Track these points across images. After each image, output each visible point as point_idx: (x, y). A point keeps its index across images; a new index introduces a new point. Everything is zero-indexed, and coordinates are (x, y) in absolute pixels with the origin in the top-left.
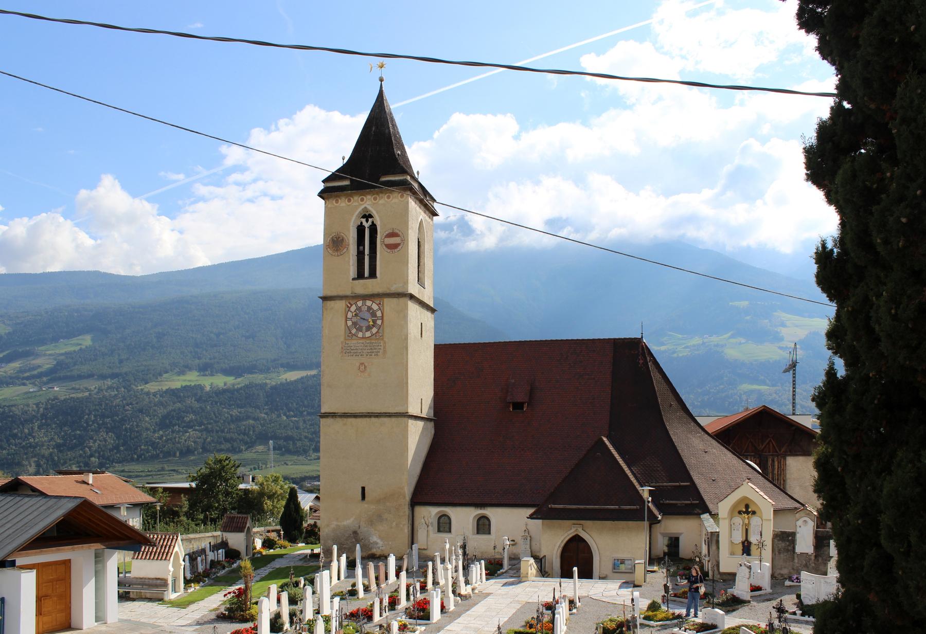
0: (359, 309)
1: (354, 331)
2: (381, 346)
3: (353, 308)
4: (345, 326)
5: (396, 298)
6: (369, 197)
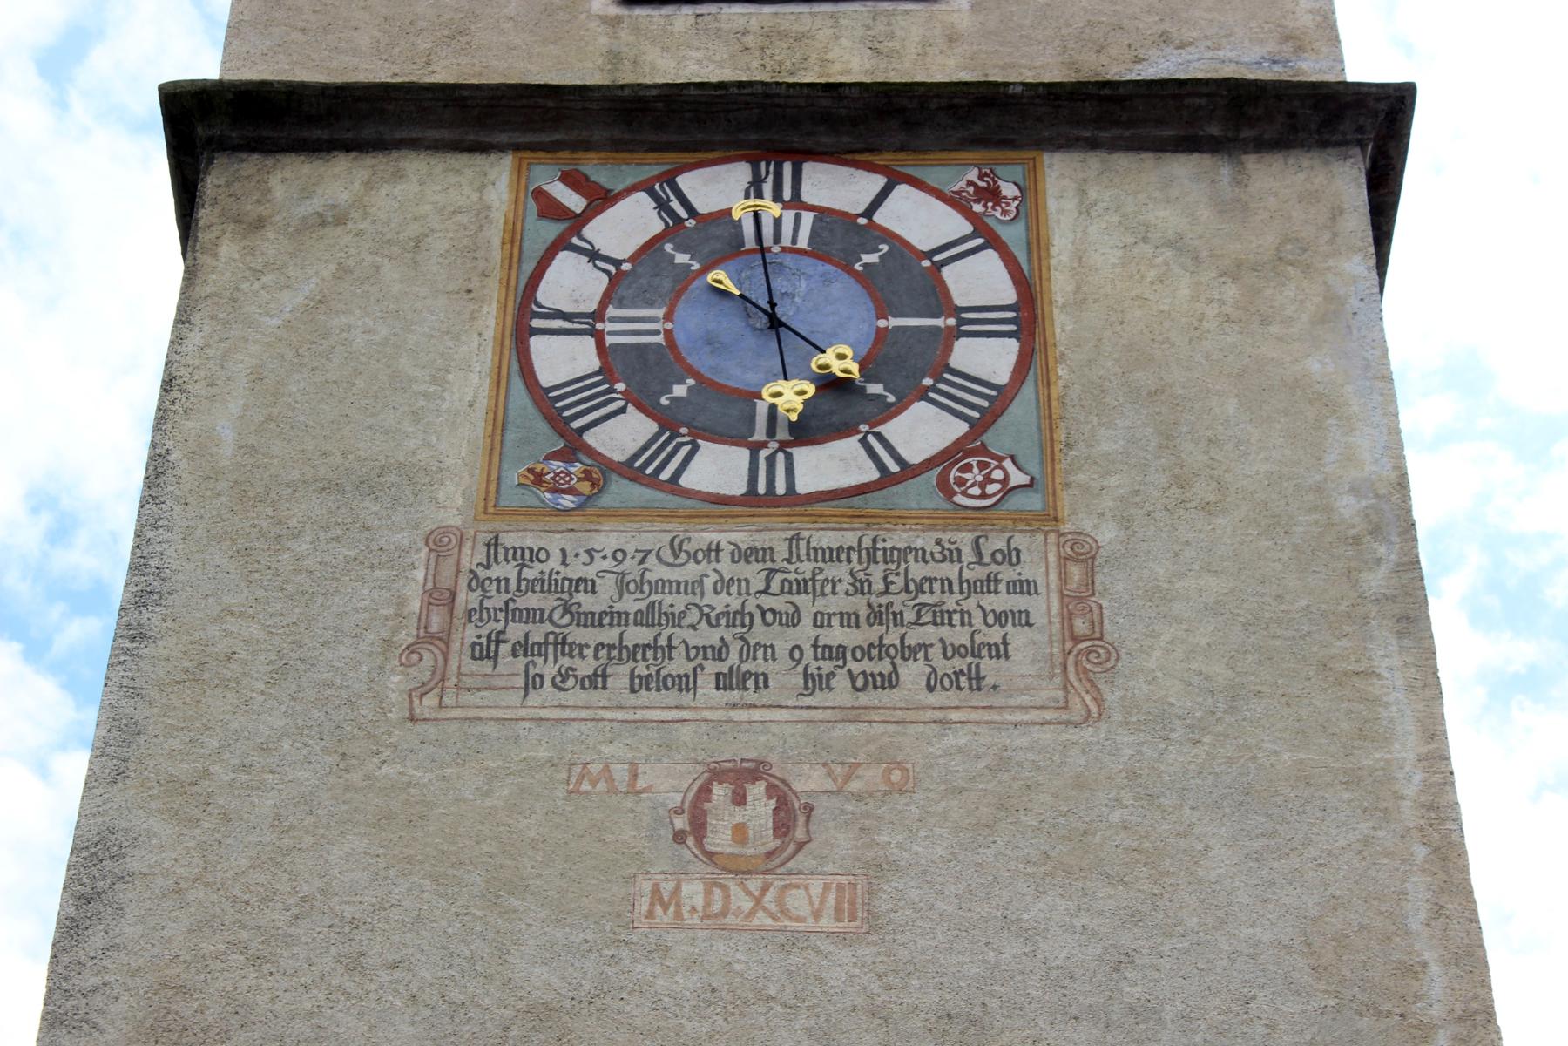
2: (1024, 587)
4: (499, 380)
5: (1212, 146)
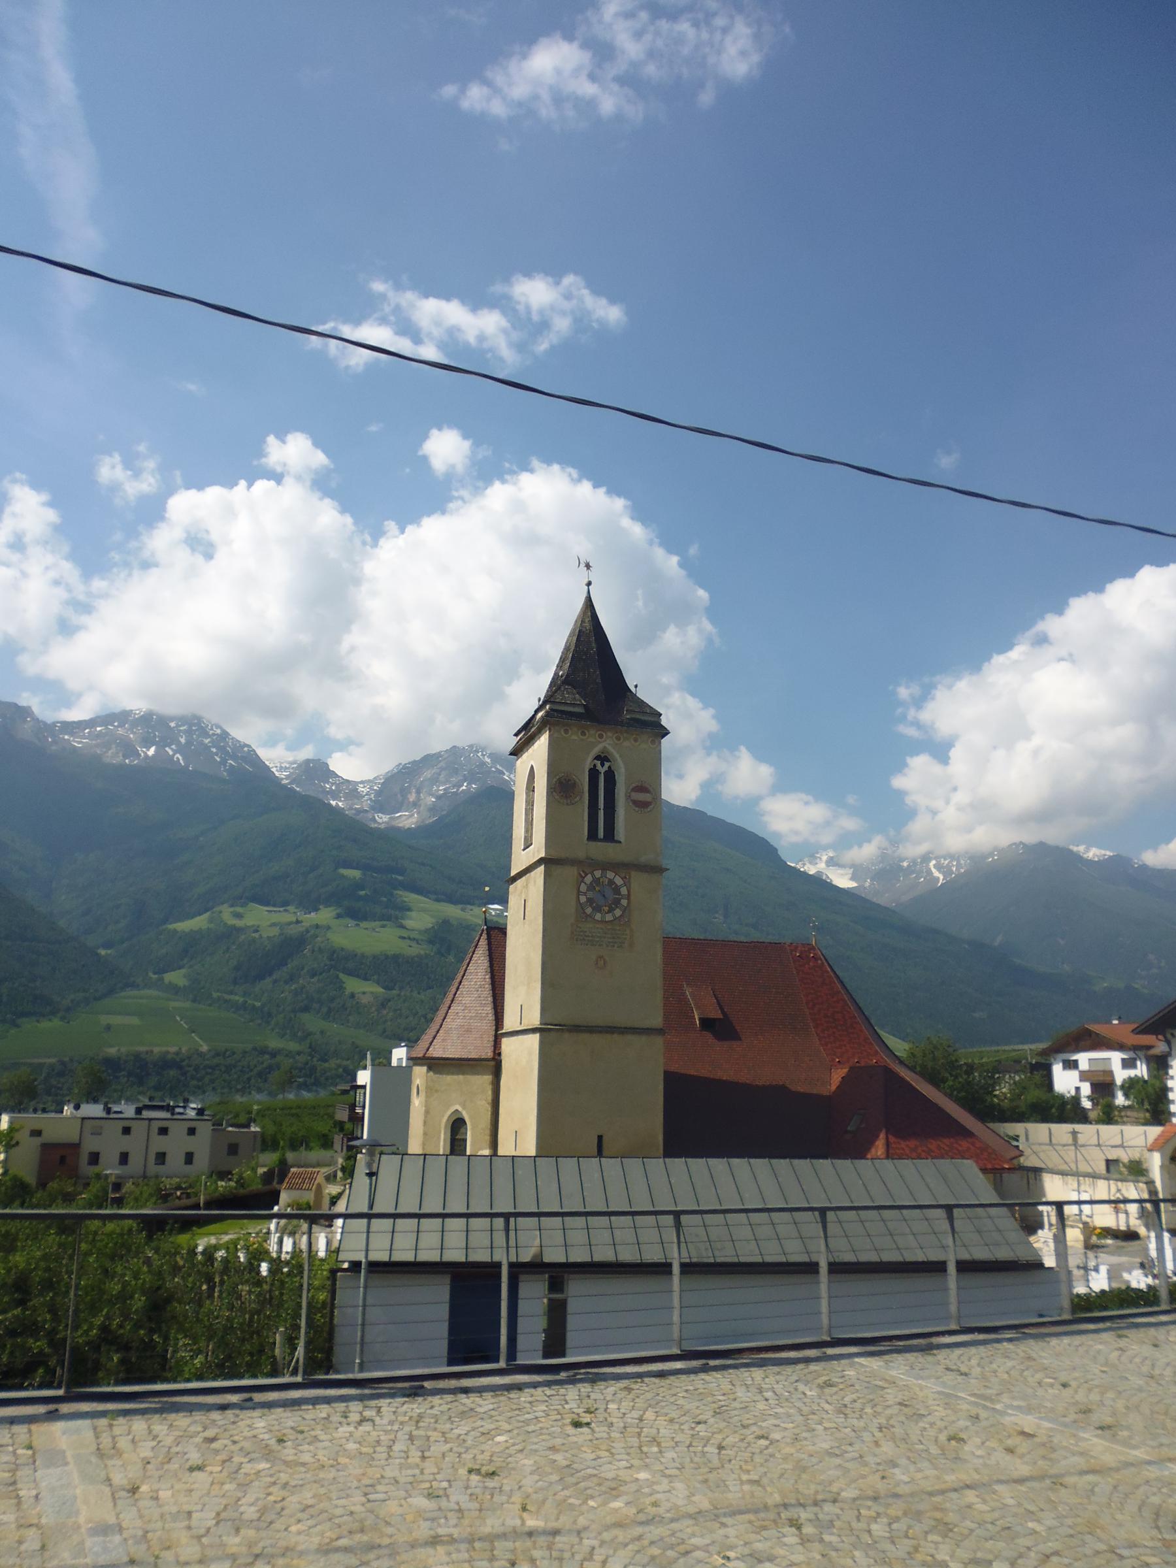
0: (596, 881)
1: (589, 910)
3: (589, 879)
6: (609, 734)
